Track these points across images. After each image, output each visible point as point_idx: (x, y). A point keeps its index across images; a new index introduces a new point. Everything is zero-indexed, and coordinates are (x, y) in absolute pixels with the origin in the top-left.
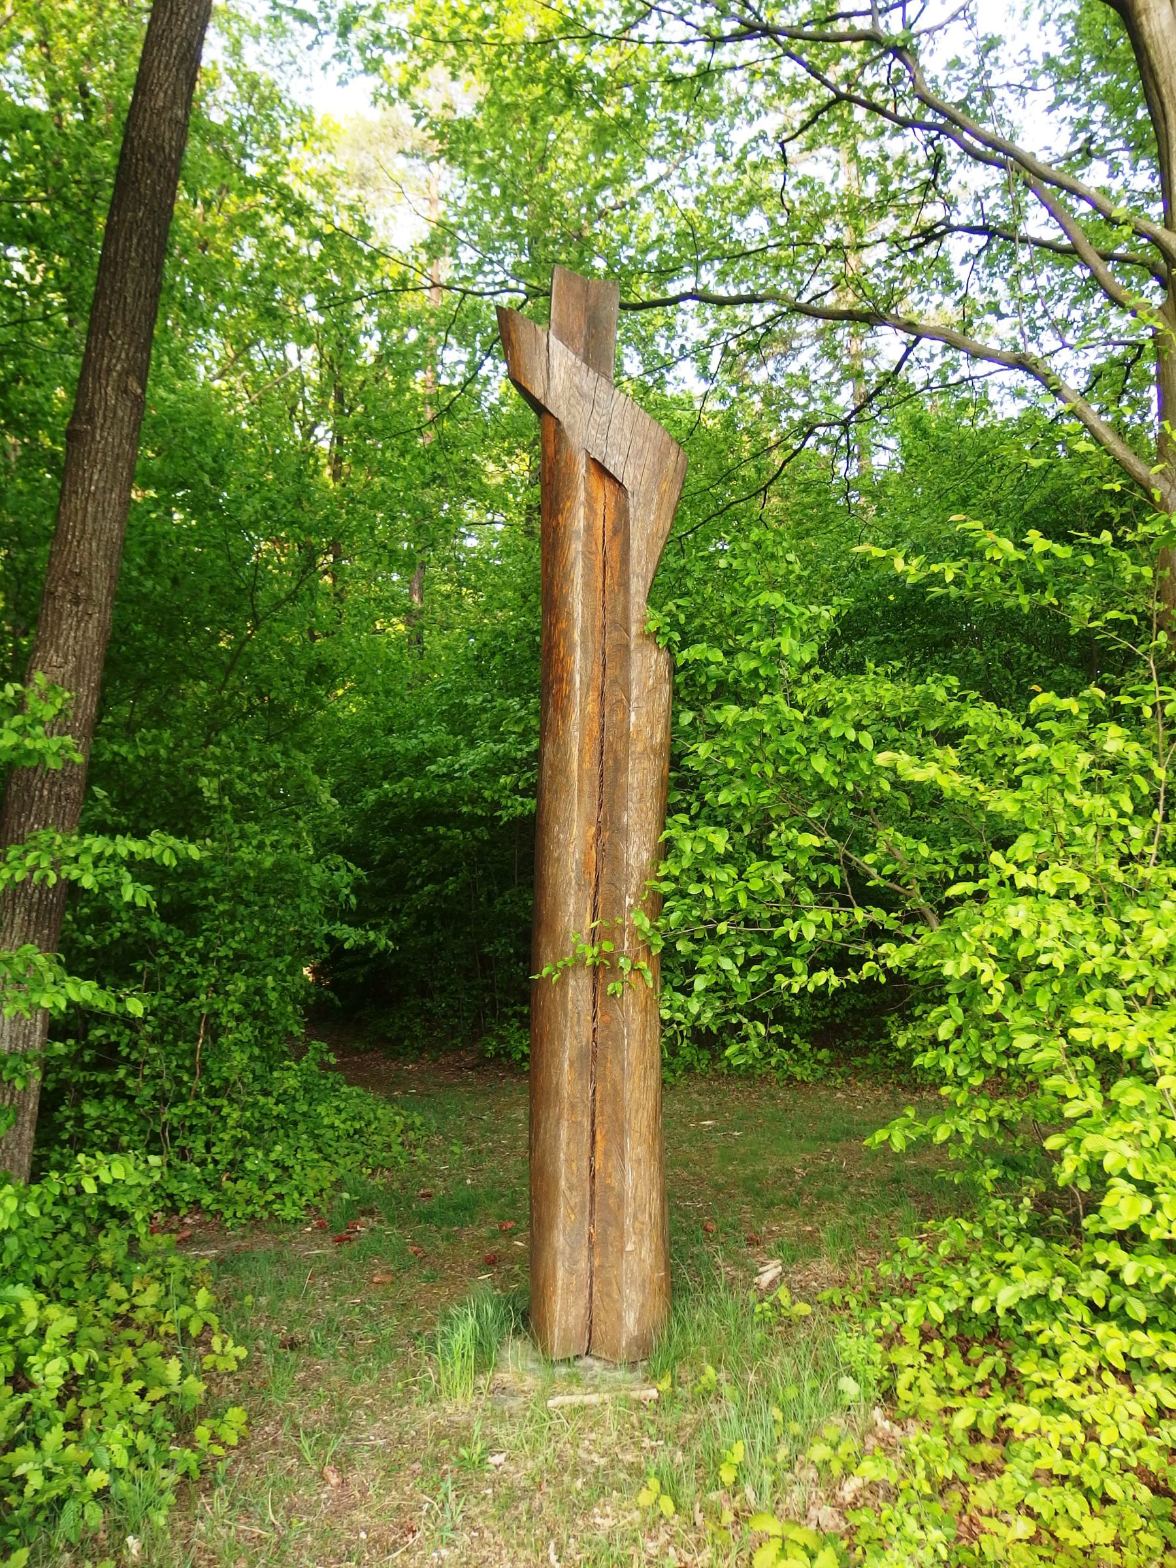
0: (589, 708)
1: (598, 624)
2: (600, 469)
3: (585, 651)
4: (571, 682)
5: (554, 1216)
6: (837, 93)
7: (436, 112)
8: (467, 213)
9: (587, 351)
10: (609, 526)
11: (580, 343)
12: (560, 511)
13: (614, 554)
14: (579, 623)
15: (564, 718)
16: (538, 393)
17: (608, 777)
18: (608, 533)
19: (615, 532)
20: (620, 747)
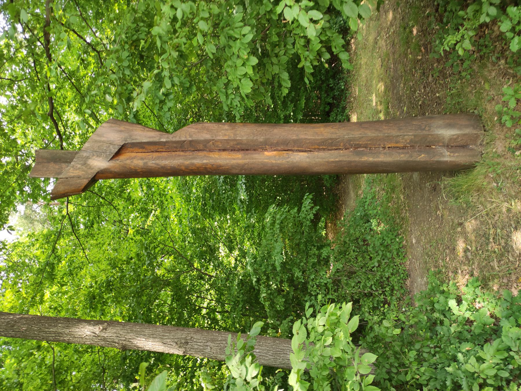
0: (217, 156)
1: (182, 153)
2: (118, 153)
3: (194, 158)
4: (207, 164)
5: (382, 162)
6: (88, 127)
7: (320, 21)
8: (187, 91)
9: (67, 162)
10: (140, 150)
11: (64, 165)
12: (136, 170)
13: (152, 148)
14: (181, 161)
15: (221, 166)
16: (85, 182)
17: (244, 147)
18: (144, 150)
19: (143, 148)
20: (232, 143)
